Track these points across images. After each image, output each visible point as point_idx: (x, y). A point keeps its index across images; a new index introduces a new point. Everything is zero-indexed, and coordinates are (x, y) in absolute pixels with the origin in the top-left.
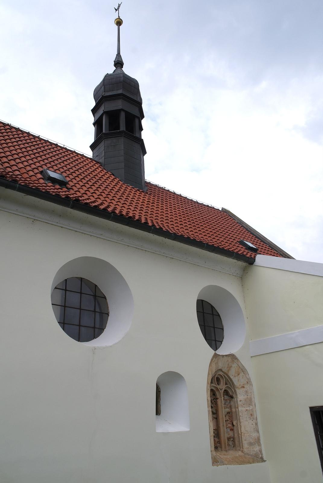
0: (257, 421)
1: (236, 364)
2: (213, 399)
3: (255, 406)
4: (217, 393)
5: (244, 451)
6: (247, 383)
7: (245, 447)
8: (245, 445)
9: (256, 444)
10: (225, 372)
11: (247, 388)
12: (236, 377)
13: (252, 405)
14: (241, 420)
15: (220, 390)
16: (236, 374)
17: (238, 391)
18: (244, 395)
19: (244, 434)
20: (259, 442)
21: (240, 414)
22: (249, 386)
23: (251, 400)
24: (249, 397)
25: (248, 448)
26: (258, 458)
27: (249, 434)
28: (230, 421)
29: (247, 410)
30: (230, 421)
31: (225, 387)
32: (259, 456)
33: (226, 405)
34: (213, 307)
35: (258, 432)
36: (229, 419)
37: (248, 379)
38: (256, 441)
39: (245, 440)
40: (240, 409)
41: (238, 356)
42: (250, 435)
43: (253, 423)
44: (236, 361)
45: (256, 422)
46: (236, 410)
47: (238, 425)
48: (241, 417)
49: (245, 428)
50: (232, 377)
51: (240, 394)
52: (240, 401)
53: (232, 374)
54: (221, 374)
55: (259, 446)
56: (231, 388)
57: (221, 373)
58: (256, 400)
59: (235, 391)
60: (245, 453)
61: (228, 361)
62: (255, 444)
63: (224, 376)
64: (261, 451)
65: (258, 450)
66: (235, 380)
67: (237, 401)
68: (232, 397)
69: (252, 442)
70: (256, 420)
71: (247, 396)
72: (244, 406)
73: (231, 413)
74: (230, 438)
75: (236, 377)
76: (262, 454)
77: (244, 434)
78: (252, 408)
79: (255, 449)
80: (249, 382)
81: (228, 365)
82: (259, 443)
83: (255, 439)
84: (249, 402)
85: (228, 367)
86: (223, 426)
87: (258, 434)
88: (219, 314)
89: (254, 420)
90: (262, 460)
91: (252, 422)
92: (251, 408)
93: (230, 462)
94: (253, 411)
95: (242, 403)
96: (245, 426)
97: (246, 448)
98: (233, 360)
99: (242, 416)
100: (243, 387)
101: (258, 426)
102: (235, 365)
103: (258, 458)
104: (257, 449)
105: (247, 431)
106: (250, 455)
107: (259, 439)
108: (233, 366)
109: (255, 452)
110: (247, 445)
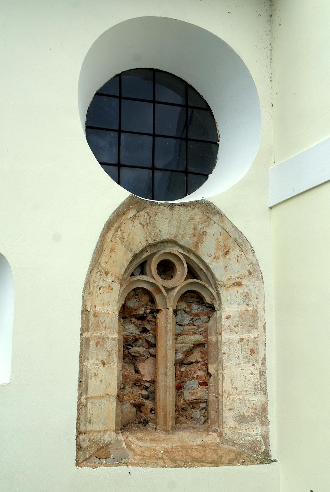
0: (265, 367)
3: (265, 332)
4: (157, 298)
5: (224, 435)
6: (250, 273)
8: (229, 419)
11: (247, 286)
12: (219, 259)
13: (257, 328)
14: (226, 363)
15: (163, 291)
16: (220, 253)
17: (223, 293)
18: (239, 304)
20: (265, 416)
21: (225, 349)
22: (254, 281)
23: (255, 315)
24: (250, 308)
25: (236, 428)
27: (241, 397)
28: (203, 363)
29: (242, 340)
30: (203, 365)
31: (183, 285)
32: (260, 449)
33: (195, 327)
34: (191, 87)
35: (265, 393)
36: (200, 360)
37: (251, 264)
38: (256, 414)
39: (230, 410)
40: (225, 336)
41: (220, 206)
42: (243, 397)
43: (255, 372)
44: (216, 218)
45: (262, 369)
48: (224, 357)
50: (207, 260)
51: (228, 300)
52: (228, 318)
53: (207, 252)
54: (177, 253)
56: (207, 285)
57: (175, 250)
58: (270, 317)
59: (218, 294)
60: (227, 438)
61: (192, 219)
64: (265, 438)
66: (218, 269)
67: (220, 318)
68: (213, 309)
69: (247, 414)
70: (264, 363)
71: (248, 305)
72: (236, 329)
73: (206, 345)
75: (221, 260)
76: (267, 445)
79: (253, 433)
80: (254, 271)
81: (195, 229)
82: (263, 419)
83: (256, 409)
84: (251, 319)
85: (194, 235)
86: (166, 374)
87: (263, 399)
88: (207, 104)
89: (256, 365)
91: (253, 369)
92: (254, 334)
93: (146, 460)
94: (257, 343)
96: (234, 375)
98: (208, 217)
99: (229, 355)
100: (239, 284)
101: (265, 379)
102: (213, 230)
103: (258, 452)
104: (256, 431)
107: (264, 409)
108: (210, 231)
110: (232, 421)
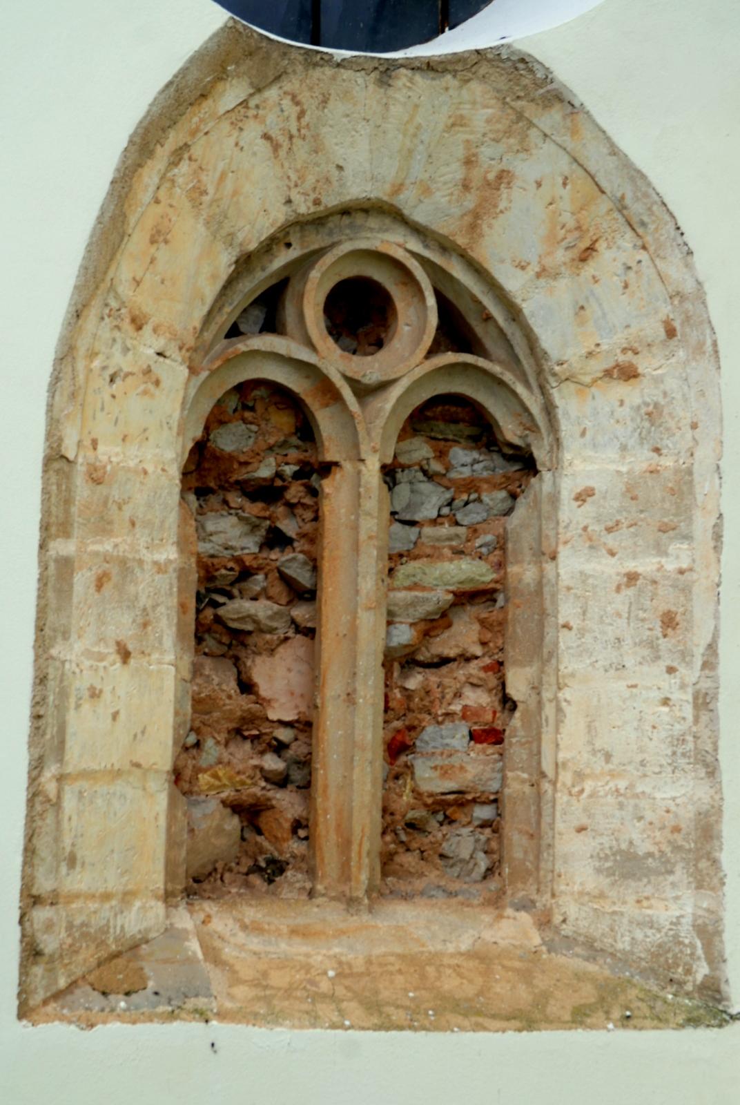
1: (553, 147)
2: (289, 470)
3: (717, 549)
5: (557, 919)
6: (671, 333)
7: (577, 888)
8: (576, 864)
9: (679, 869)
10: (443, 231)
11: (658, 380)
12: (556, 276)
14: (569, 663)
16: (561, 256)
17: (567, 402)
18: (624, 448)
19: (580, 776)
21: (567, 611)
22: (686, 363)
23: (682, 488)
24: (667, 462)
26: (681, 984)
27: (622, 784)
28: (487, 661)
29: (632, 578)
32: (688, 971)
33: (461, 531)
36: (478, 650)
37: (677, 296)
38: (677, 848)
39: (581, 829)
40: (571, 564)
41: (567, 71)
42: (631, 786)
43: (676, 696)
44: (550, 119)
45: (705, 685)
46: (541, 570)
47: (540, 704)
48: (566, 640)
49: (590, 728)
50: (512, 282)
51: (583, 434)
52: (582, 497)
53: (514, 251)
54: (399, 254)
55: (699, 887)
56: (508, 377)
57: (396, 242)
59: (549, 409)
60: (567, 930)
61: (458, 122)
62: (671, 872)
63: (424, 262)
64: (709, 933)
65: (687, 921)
66: (554, 315)
67: (555, 499)
68: (526, 463)
69: (643, 847)
70: (710, 664)
71: (657, 450)
72: (611, 540)
74: (461, 804)
77: (580, 776)
78: (685, 566)
79: (664, 913)
80: (684, 326)
81: (469, 162)
82: (703, 864)
83: (676, 829)
84: (668, 503)
86: (350, 698)
87: (703, 793)
89: (682, 670)
90: (710, 1007)
91: (669, 685)
92: (678, 556)
93: (270, 1003)
94: (686, 590)
95: (598, 520)
97: (581, 894)
98: (520, 116)
100: (628, 374)
101: (714, 721)
102: (540, 166)
103: (681, 984)
104: (674, 907)
105: (608, 757)
106: (612, 955)
109: (656, 937)
